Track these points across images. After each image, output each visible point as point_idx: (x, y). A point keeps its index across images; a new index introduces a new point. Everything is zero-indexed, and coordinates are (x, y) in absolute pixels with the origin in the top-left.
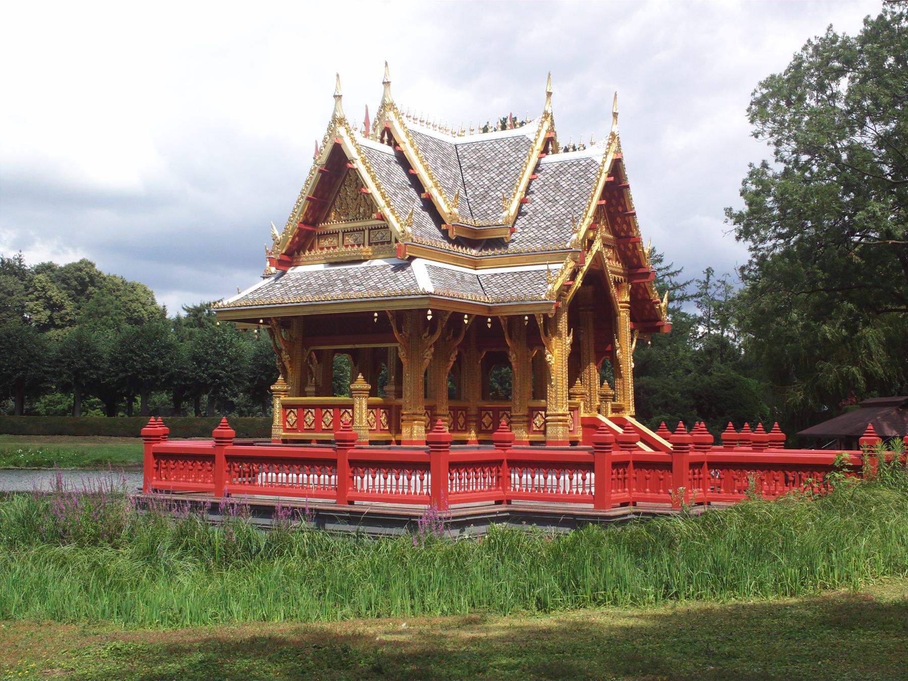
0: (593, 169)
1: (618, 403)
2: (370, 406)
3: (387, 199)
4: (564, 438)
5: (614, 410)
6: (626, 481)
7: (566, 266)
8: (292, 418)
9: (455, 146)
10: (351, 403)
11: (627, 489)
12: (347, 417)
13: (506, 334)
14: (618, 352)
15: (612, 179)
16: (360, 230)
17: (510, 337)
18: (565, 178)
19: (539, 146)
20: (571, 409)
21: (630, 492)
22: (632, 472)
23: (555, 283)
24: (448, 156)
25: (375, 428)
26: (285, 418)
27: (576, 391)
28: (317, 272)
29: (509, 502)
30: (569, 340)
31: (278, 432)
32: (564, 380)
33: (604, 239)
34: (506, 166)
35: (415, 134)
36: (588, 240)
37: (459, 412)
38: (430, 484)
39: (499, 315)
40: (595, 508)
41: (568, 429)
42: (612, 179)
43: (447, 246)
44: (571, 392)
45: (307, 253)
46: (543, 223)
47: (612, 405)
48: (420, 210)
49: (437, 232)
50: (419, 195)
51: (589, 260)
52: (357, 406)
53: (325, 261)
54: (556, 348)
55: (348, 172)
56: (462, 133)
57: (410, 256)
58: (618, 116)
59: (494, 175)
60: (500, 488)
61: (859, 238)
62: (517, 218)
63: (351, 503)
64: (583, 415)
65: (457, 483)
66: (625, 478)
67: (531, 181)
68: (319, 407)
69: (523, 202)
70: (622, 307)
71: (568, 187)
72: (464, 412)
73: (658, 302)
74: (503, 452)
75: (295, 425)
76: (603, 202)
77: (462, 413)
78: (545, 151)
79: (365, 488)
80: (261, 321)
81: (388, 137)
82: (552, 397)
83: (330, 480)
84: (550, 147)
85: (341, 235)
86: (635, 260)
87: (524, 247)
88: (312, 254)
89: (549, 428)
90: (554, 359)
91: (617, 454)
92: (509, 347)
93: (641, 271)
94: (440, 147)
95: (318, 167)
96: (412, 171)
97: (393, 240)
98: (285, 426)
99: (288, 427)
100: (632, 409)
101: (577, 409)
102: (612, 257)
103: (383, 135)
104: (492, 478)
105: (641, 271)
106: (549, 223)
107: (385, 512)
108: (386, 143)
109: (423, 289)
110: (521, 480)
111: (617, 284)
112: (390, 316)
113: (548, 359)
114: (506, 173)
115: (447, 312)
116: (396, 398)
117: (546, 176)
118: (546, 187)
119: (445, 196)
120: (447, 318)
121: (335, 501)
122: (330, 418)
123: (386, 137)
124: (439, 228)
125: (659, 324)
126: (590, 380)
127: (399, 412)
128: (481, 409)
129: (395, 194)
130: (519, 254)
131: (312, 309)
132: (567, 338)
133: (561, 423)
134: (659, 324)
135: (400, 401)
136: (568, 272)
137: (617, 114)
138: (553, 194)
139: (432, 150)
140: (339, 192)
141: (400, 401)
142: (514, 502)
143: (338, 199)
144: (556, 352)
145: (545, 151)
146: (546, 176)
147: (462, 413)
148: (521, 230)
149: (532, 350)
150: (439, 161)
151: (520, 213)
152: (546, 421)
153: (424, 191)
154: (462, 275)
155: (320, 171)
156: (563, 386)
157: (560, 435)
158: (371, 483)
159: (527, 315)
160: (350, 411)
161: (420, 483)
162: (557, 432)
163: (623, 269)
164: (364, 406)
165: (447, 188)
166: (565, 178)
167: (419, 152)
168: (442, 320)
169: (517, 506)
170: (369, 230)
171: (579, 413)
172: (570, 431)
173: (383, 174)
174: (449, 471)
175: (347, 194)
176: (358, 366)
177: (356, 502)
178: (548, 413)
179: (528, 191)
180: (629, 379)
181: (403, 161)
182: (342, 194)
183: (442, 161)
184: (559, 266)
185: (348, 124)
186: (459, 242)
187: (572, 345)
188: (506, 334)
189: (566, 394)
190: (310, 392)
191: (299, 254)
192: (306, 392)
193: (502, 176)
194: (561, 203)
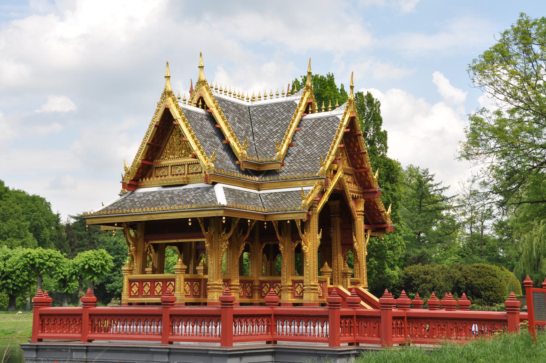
0: (336, 124)
1: (356, 279)
2: (186, 280)
3: (199, 145)
4: (314, 301)
5: (352, 283)
6: (403, 329)
7: (315, 187)
8: (135, 289)
9: (249, 107)
10: (173, 277)
11: (403, 335)
12: (171, 287)
13: (277, 233)
14: (355, 244)
15: (349, 130)
16: (182, 165)
17: (280, 234)
18: (318, 130)
19: (302, 108)
20: (320, 282)
21: (354, 336)
22: (405, 325)
23: (307, 200)
24: (243, 115)
25: (189, 294)
26: (130, 288)
27: (324, 270)
28: (154, 192)
29: (275, 342)
30: (319, 237)
31: (125, 297)
32: (315, 263)
33: (344, 169)
34: (280, 122)
35: (221, 100)
36: (334, 171)
37: (247, 284)
38: (328, 331)
39: (272, 220)
40: (162, 343)
41: (318, 295)
42: (349, 130)
43: (239, 175)
44: (321, 270)
45: (148, 179)
46: (303, 160)
47: (351, 280)
48: (222, 152)
49: (233, 166)
50: (221, 141)
51: (332, 184)
52: (177, 280)
53: (159, 185)
54: (310, 241)
55: (174, 127)
56: (253, 100)
57: (213, 182)
58: (354, 88)
59: (272, 127)
60: (270, 333)
61: (532, 167)
62: (286, 156)
63: (171, 343)
64: (329, 286)
65: (239, 329)
66: (351, 327)
67: (295, 132)
68: (153, 281)
69: (290, 145)
70: (358, 215)
71: (320, 136)
72: (250, 284)
73: (383, 212)
74: (404, 311)
75: (137, 293)
76: (342, 146)
77: (249, 285)
78: (307, 112)
79: (317, 334)
80: (116, 225)
81: (201, 103)
82: (307, 274)
83: (158, 329)
84: (310, 109)
85: (170, 168)
86: (367, 183)
87: (289, 176)
88: (151, 180)
89: (305, 294)
90: (308, 249)
91: (344, 310)
92: (279, 241)
93: (371, 190)
94: (239, 110)
95: (155, 123)
96: (217, 126)
97: (203, 172)
98: (130, 294)
99: (132, 294)
100: (366, 283)
101: (325, 282)
102: (351, 181)
103: (198, 102)
104: (264, 326)
105: (371, 190)
106: (306, 160)
107: (192, 348)
108: (200, 107)
109: (220, 203)
110: (284, 328)
111: (354, 199)
112: (200, 221)
113: (304, 248)
114: (280, 126)
115: (237, 218)
116: (204, 274)
117: (306, 128)
118: (306, 136)
119: (238, 142)
120: (237, 222)
121: (160, 342)
122: (145, 289)
123: (200, 103)
124: (234, 162)
125: (385, 226)
126: (338, 263)
127: (206, 283)
128: (262, 282)
129: (205, 141)
130: (286, 180)
131: (149, 216)
132: (318, 235)
133: (216, 290)
134: (385, 226)
135: (206, 276)
136: (317, 191)
137: (353, 87)
138: (310, 140)
139: (232, 111)
140: (169, 139)
141: (206, 276)
142: (360, 345)
143: (168, 145)
144: (310, 244)
145: (307, 112)
146: (306, 128)
147: (249, 285)
148: (289, 164)
149: (294, 243)
150: (236, 119)
151: (287, 154)
152: (303, 290)
153: (225, 139)
154: (249, 193)
155: (156, 126)
156: (314, 267)
157: (312, 299)
158: (320, 331)
159: (289, 220)
160: (173, 283)
161: (215, 329)
162: (309, 297)
163: (358, 189)
164: (182, 280)
165: (241, 137)
166: (318, 130)
167: (222, 113)
168: (234, 223)
169: (362, 347)
170: (188, 165)
171: (326, 285)
172: (319, 297)
173: (198, 128)
174: (234, 321)
175: (174, 141)
176: (182, 254)
177: (174, 343)
178: (304, 284)
179: (293, 138)
180: (364, 263)
181: (211, 118)
182: (171, 141)
183: (239, 118)
184: (311, 188)
185: (174, 95)
186: (247, 172)
187: (321, 240)
188: (277, 233)
189: (316, 272)
190: (148, 271)
191: (142, 180)
192: (146, 272)
193: (277, 128)
194: (315, 146)
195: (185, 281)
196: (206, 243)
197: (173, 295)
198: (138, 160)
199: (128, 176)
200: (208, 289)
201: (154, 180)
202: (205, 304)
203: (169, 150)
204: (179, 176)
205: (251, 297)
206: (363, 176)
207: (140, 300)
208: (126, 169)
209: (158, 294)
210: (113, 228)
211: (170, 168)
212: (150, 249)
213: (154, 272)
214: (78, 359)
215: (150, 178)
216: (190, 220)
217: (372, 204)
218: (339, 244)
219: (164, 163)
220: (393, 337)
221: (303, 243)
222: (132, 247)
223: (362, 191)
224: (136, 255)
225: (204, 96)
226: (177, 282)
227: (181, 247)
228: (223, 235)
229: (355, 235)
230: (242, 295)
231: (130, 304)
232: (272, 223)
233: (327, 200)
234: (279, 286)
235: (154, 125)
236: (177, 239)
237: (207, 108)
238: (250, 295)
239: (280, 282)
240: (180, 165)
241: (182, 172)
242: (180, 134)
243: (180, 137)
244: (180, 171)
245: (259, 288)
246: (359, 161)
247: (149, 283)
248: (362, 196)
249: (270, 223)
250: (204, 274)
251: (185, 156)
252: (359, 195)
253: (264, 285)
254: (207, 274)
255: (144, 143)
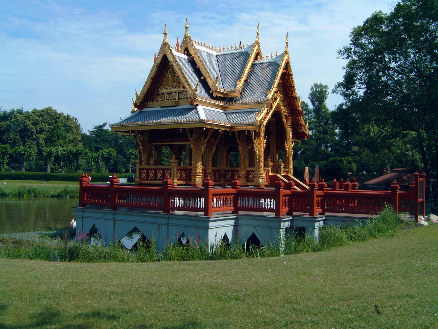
2: (178, 170)
8: (144, 175)
16: (174, 93)
17: (239, 140)
23: (259, 117)
30: (265, 142)
36: (274, 98)
47: (283, 170)
51: (274, 106)
52: (172, 169)
58: (288, 44)
68: (156, 170)
75: (145, 177)
85: (166, 94)
92: (238, 144)
95: (156, 65)
97: (189, 97)
100: (292, 172)
112: (187, 130)
116: (189, 166)
120: (212, 131)
123: (186, 52)
128: (226, 171)
135: (191, 167)
140: (165, 76)
141: (191, 167)
143: (165, 79)
147: (218, 173)
158: (178, 203)
160: (169, 171)
168: (210, 132)
170: (178, 93)
175: (169, 77)
176: (173, 152)
191: (147, 103)
195: (177, 170)
196: (191, 145)
197: (253, 181)
198: (145, 89)
199: (138, 100)
200: (192, 176)
201: (155, 103)
202: (190, 185)
203: (165, 83)
204: (173, 100)
205: (219, 181)
206: (292, 102)
207: (153, 182)
208: (137, 95)
209: (159, 178)
210: (128, 134)
211: (166, 94)
212: (152, 149)
213: (155, 164)
214: (147, 222)
215: (152, 101)
216: (246, 132)
217: (297, 120)
218: (275, 146)
219: (162, 91)
220: (316, 209)
221: (255, 146)
222: (141, 147)
223: (291, 112)
224: (143, 152)
225: (188, 47)
226: (172, 171)
227: (171, 147)
228: (202, 140)
229: (286, 141)
230: (213, 179)
231: (141, 184)
232: (234, 133)
233: (270, 117)
234: (237, 174)
235: (156, 66)
236: (171, 142)
237: (191, 55)
238: (218, 179)
239: (238, 171)
240: (173, 93)
241: (174, 97)
242: (173, 72)
243: (173, 74)
244: (173, 96)
245: (206, 175)
246: (290, 92)
247: (153, 171)
248: (290, 115)
249: (233, 132)
250: (189, 166)
251: (177, 87)
252: (289, 115)
253: (227, 173)
254: (191, 166)
255: (149, 78)
